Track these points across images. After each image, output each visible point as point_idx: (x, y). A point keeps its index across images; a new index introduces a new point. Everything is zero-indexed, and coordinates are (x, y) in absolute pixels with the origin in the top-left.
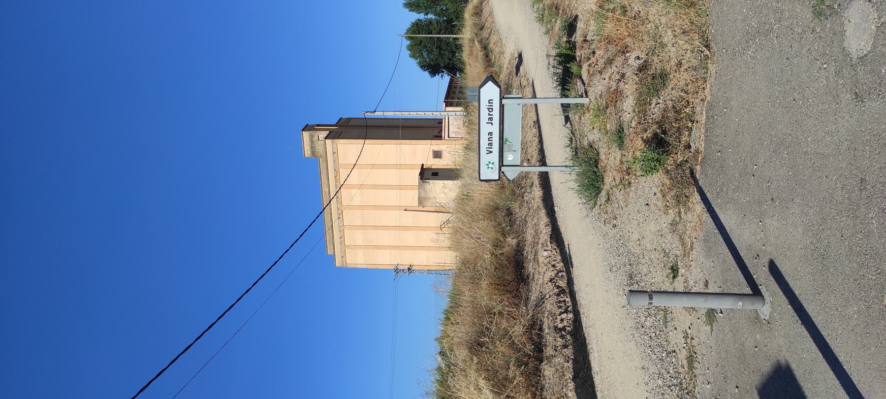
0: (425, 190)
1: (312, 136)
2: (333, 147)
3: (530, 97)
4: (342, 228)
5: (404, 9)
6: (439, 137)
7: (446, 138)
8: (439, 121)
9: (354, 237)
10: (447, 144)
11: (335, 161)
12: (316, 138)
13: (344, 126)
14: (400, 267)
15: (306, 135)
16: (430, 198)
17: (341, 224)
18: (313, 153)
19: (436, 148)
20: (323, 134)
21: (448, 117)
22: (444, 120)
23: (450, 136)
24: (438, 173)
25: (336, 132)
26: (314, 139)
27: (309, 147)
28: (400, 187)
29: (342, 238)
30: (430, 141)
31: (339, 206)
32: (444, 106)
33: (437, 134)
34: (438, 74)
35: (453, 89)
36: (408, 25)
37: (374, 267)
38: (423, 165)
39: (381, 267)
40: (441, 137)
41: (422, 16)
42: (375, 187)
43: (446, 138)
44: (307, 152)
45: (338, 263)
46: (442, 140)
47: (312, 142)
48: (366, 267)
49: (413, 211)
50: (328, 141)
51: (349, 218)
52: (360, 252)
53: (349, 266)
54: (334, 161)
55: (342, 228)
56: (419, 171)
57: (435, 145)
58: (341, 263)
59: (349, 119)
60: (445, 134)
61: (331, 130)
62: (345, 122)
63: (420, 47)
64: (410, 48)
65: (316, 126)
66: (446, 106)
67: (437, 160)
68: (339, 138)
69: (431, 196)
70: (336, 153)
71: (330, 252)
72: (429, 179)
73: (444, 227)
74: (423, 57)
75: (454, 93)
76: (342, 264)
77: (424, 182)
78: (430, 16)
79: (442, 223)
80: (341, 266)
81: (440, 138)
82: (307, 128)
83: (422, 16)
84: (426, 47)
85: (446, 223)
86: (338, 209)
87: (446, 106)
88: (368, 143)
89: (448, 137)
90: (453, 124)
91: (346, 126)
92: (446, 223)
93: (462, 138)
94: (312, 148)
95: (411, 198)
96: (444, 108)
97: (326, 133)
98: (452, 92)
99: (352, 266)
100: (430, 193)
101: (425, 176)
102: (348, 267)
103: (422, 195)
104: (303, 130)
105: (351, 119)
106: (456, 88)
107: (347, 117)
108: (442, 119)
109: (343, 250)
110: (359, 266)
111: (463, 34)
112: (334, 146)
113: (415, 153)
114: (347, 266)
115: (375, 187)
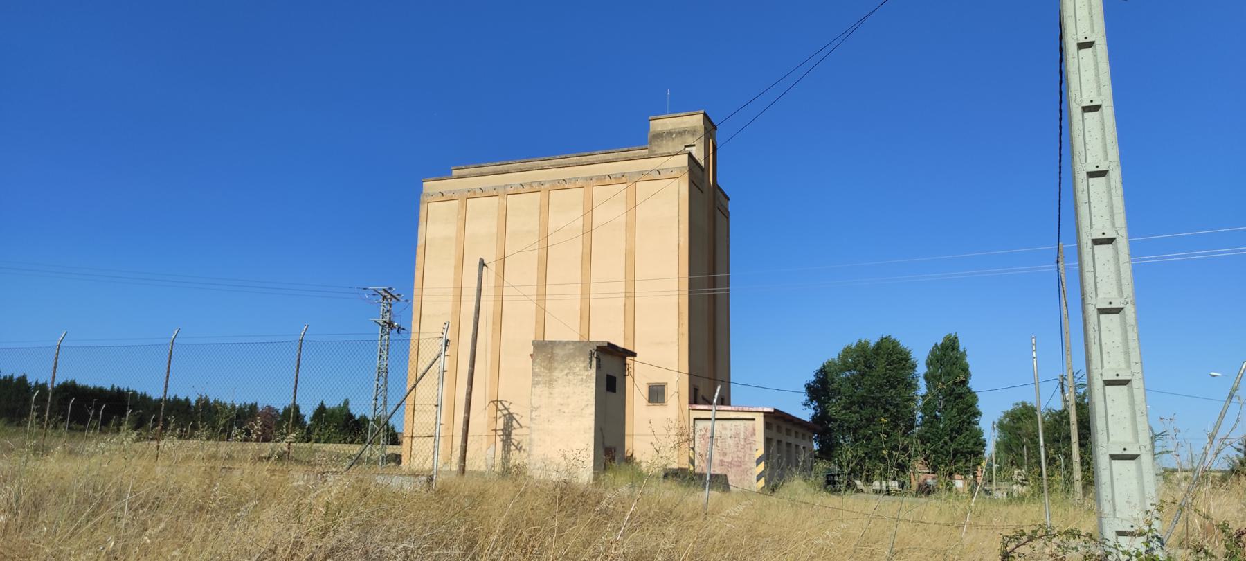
0: (571, 356)
1: (693, 132)
4: (501, 191)
6: (696, 397)
7: (694, 414)
9: (483, 213)
10: (681, 419)
11: (643, 176)
12: (690, 141)
13: (714, 204)
14: (397, 307)
15: (696, 121)
16: (551, 369)
17: (511, 191)
18: (659, 136)
19: (670, 391)
20: (699, 154)
21: (710, 419)
23: (696, 422)
24: (614, 391)
25: (703, 181)
26: (687, 136)
27: (670, 127)
29: (483, 193)
30: (687, 372)
31: (547, 186)
32: (766, 410)
33: (701, 393)
36: (905, 343)
37: (419, 260)
38: (634, 354)
39: (418, 274)
40: (696, 403)
41: (921, 369)
42: (587, 258)
43: (694, 414)
44: (658, 125)
45: (430, 186)
46: (690, 403)
47: (681, 133)
48: (421, 242)
49: (480, 290)
50: (684, 160)
51: (523, 209)
52: (451, 230)
53: (423, 208)
54: (642, 173)
55: (501, 191)
56: (620, 344)
57: (677, 384)
58: (431, 192)
59: (726, 215)
60: (702, 411)
63: (861, 367)
64: (862, 348)
65: (713, 143)
66: (766, 414)
69: (556, 374)
70: (659, 177)
71: (455, 173)
72: (599, 367)
73: (498, 410)
74: (842, 371)
75: (788, 432)
76: (429, 195)
77: (591, 354)
78: (922, 388)
79: (507, 405)
80: (424, 191)
82: (710, 127)
83: (921, 369)
84: (863, 375)
85: (505, 412)
86: (541, 183)
87: (766, 414)
88: (681, 243)
89: (695, 419)
90: (725, 428)
91: (714, 207)
92: (505, 412)
93: (693, 449)
94: (670, 133)
95: (563, 329)
96: (760, 409)
97: (699, 154)
98: (789, 426)
99: (423, 214)
100: (562, 371)
101: (606, 360)
102: (421, 206)
103: (559, 352)
104: (705, 114)
105: (728, 218)
106: (796, 437)
108: (729, 404)
109: (457, 195)
110: (421, 229)
111: (46, 383)
112: (675, 172)
114: (424, 202)
115: (587, 258)
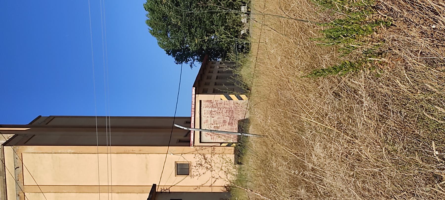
2: (15, 159)
3: (237, 132)
5: (145, 23)
7: (197, 142)
8: (186, 120)
19: (181, 159)
22: (193, 118)
28: (254, 14)
32: (194, 93)
33: (182, 138)
34: (187, 62)
35: (205, 80)
38: (154, 186)
43: (197, 142)
46: (190, 146)
50: (8, 150)
60: (195, 137)
61: (17, 133)
62: (45, 121)
67: (181, 177)
68: (26, 143)
70: (20, 169)
81: (188, 144)
89: (200, 142)
90: (207, 121)
93: (221, 143)
96: (194, 96)
105: (54, 117)
107: (49, 116)
113: (146, 168)
